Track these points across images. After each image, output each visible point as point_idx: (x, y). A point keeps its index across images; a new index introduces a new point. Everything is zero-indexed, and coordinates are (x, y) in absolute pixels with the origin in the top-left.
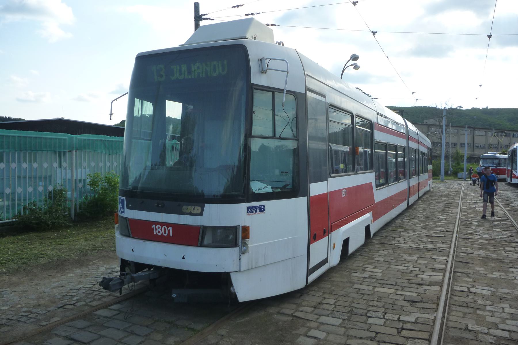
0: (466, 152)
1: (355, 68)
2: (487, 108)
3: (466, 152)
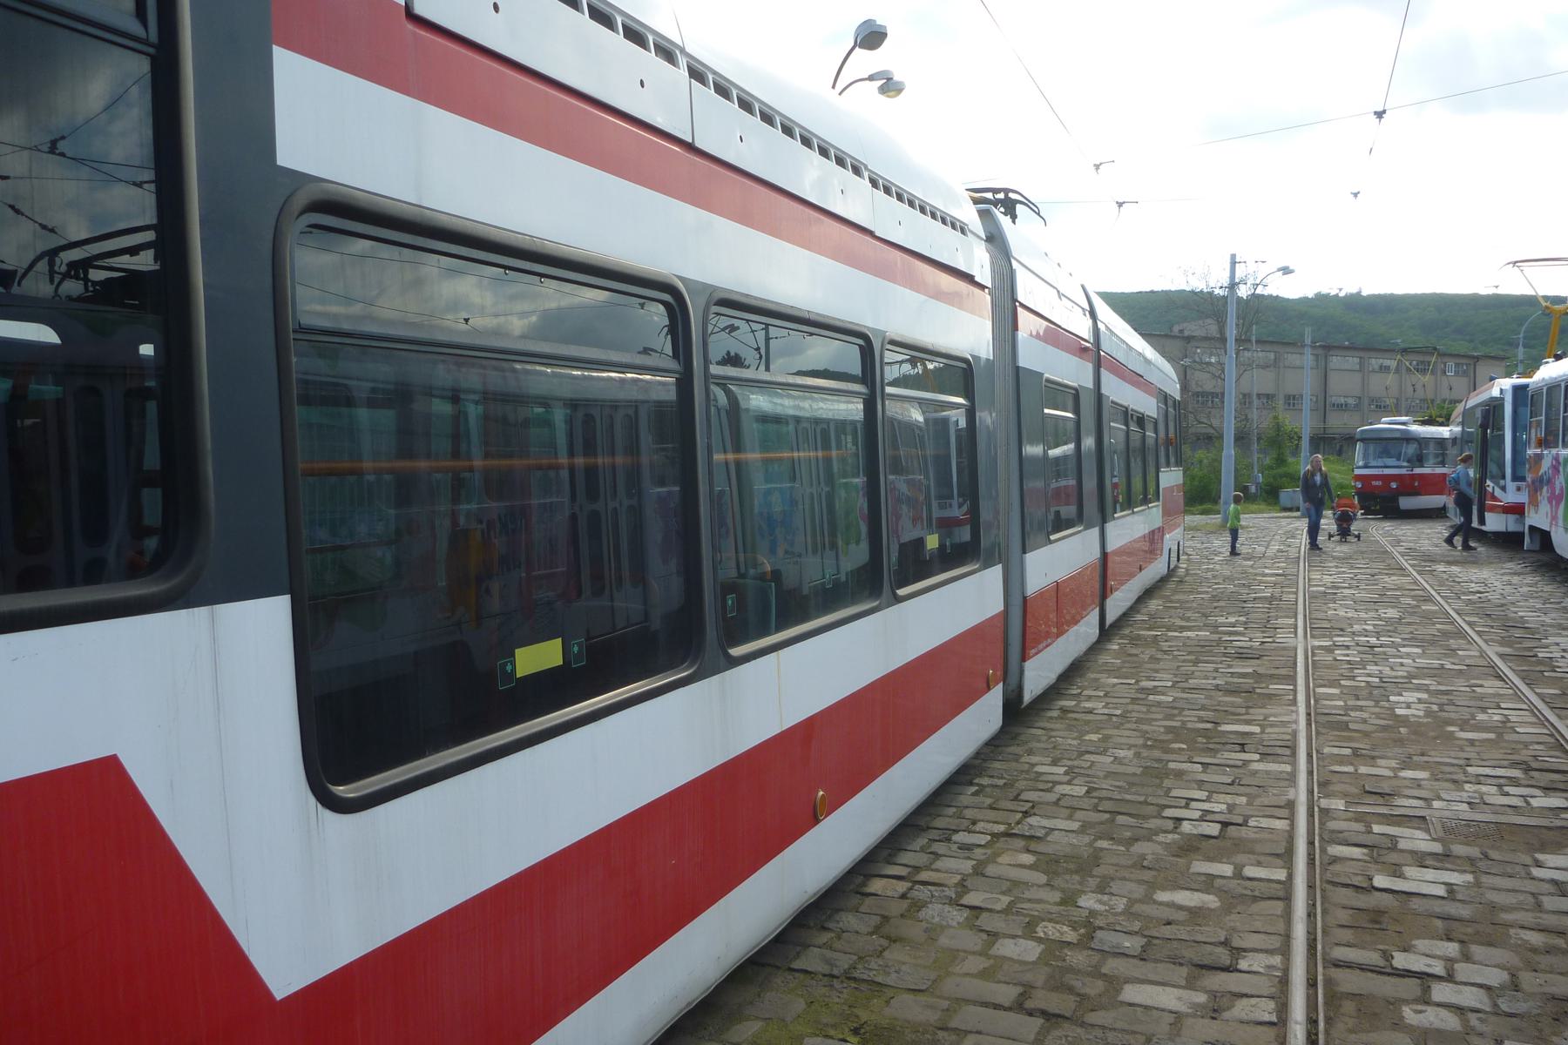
0: (1305, 423)
1: (884, 90)
2: (1359, 294)
3: (1305, 423)
